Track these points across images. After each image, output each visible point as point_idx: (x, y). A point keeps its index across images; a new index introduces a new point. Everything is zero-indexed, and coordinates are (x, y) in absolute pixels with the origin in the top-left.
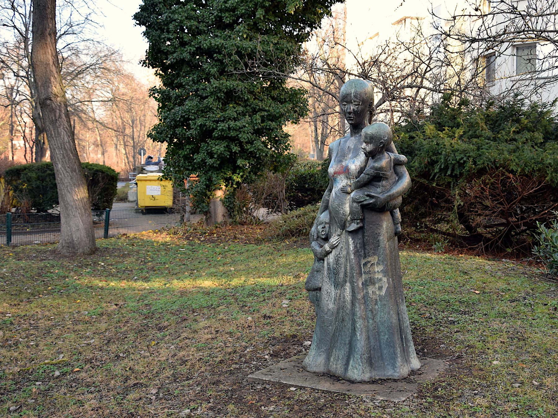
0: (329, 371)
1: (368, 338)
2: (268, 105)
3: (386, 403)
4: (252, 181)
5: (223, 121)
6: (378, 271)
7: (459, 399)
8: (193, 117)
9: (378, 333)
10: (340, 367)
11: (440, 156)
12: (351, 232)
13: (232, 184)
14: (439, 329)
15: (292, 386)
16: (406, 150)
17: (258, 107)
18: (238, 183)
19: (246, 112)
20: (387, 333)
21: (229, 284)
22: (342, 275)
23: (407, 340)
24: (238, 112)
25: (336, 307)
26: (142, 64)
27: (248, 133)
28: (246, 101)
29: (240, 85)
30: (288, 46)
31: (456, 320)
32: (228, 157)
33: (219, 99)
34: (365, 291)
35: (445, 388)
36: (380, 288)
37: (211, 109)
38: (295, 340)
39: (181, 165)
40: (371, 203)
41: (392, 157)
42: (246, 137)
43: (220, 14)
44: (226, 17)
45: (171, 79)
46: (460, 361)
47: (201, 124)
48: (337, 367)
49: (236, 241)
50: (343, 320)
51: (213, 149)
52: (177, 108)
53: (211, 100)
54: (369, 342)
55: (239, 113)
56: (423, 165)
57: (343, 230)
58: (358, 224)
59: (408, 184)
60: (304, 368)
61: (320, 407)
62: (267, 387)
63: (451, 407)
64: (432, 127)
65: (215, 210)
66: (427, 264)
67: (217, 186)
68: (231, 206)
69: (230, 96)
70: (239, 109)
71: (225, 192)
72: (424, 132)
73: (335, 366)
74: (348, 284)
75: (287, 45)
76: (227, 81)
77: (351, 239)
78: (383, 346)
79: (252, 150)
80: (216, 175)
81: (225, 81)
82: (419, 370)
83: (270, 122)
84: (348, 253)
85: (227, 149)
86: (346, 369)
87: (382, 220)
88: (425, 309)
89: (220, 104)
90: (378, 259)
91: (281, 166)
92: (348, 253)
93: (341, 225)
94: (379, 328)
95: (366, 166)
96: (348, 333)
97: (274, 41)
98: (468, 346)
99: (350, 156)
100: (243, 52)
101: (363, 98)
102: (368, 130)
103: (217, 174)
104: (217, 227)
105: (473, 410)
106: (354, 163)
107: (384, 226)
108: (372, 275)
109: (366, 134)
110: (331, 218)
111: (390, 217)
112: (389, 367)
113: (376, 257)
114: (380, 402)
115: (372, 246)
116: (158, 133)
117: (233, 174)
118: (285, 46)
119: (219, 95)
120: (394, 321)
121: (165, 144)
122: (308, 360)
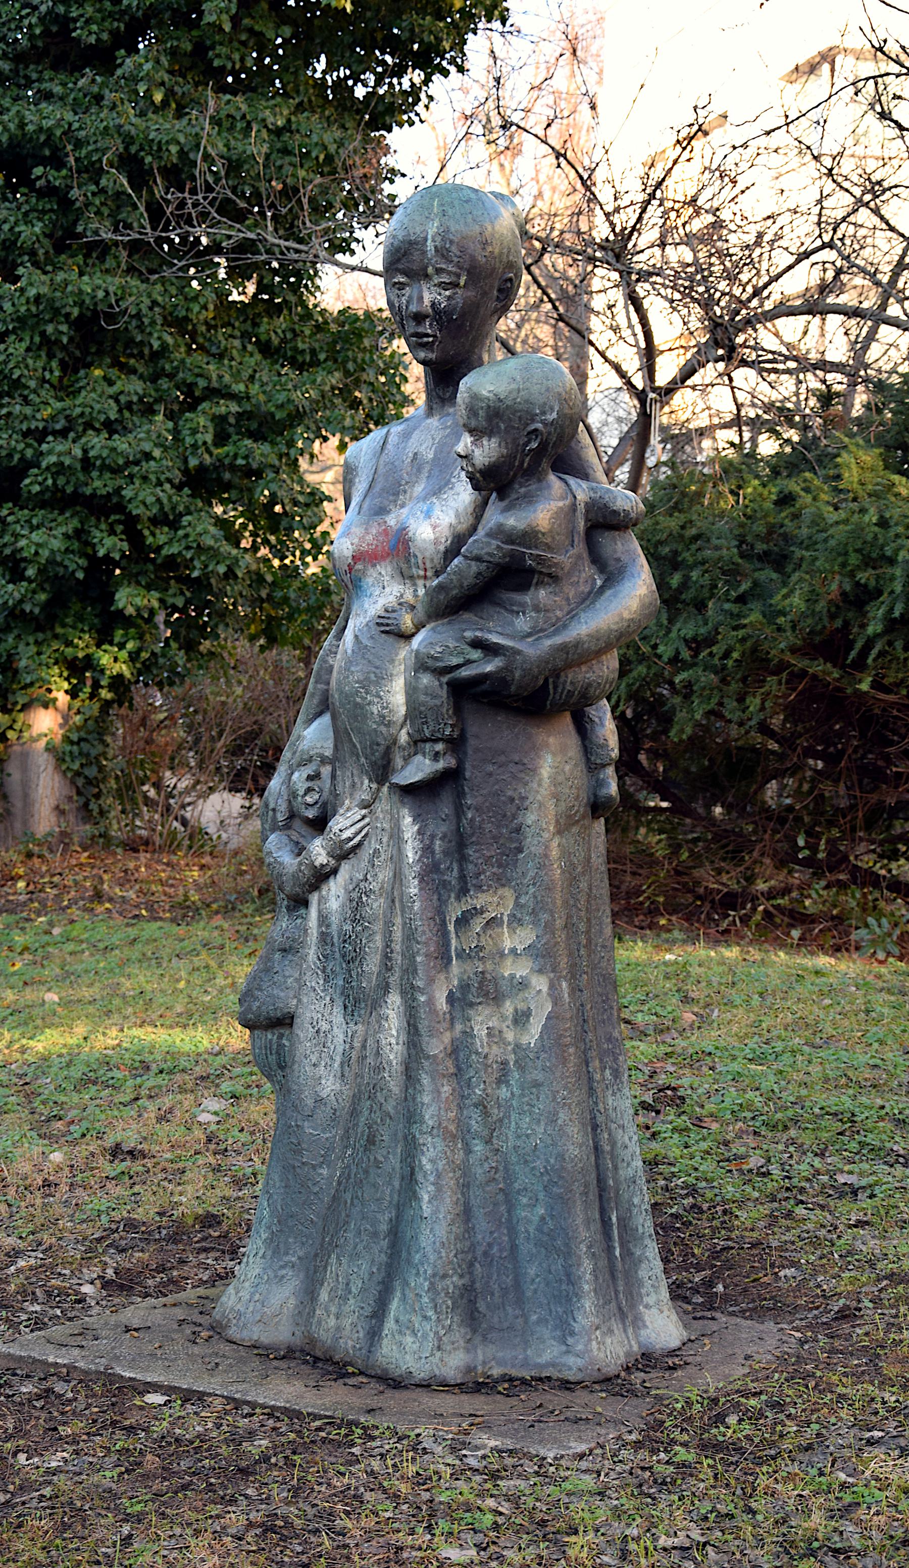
0: (312, 1341)
1: (466, 1214)
2: (245, 375)
3: (509, 1461)
4: (174, 678)
5: (63, 434)
6: (513, 951)
7: (800, 1457)
9: (508, 1197)
11: (889, 570)
12: (409, 791)
13: (96, 686)
14: (789, 1215)
15: (155, 1387)
16: (760, 547)
17: (202, 383)
18: (118, 682)
19: (158, 401)
20: (541, 1196)
21: (23, 1050)
22: (372, 964)
24: (123, 399)
25: (347, 1093)
27: (160, 484)
28: (156, 356)
29: (137, 294)
30: (327, 138)
31: (864, 1182)
32: (80, 575)
33: (48, 345)
34: (459, 1027)
35: (756, 1416)
36: (521, 1019)
37: (17, 384)
38: (217, 1237)
40: (485, 677)
41: (581, 496)
42: (150, 500)
43: (61, 9)
44: (88, 22)
46: (846, 1327)
48: (339, 1325)
49: (100, 909)
50: (371, 1141)
51: (22, 543)
54: (469, 1231)
55: (129, 406)
56: (821, 606)
57: (381, 783)
58: (436, 756)
59: (643, 606)
60: (218, 1330)
61: (244, 1464)
62: (60, 1387)
63: (763, 1481)
64: (870, 457)
65: (26, 786)
66: (802, 990)
67: (36, 692)
68: (91, 772)
69: (94, 337)
70: (130, 388)
71: (66, 718)
72: (838, 477)
73: (332, 1322)
74: (394, 999)
75: (319, 132)
76: (81, 274)
77: (408, 820)
78: (525, 1248)
79: (175, 549)
80: (33, 649)
81: (74, 276)
82: (672, 1353)
83: (248, 442)
84: (398, 877)
85: (76, 545)
86: (374, 1335)
87: (535, 749)
88: (751, 1141)
89: (54, 364)
90: (517, 904)
91: (290, 617)
92: (398, 877)
93: (373, 764)
94: (509, 1177)
95: (473, 529)
96: (389, 1192)
97: (270, 120)
98: (890, 1276)
99: (419, 489)
100: (148, 159)
101: (473, 258)
102: (482, 383)
103: (37, 643)
104: (29, 855)
105: (848, 1499)
106: (428, 515)
107: (545, 772)
108: (489, 966)
109: (475, 397)
110: (340, 736)
111: (573, 741)
112: (545, 1332)
113: (508, 893)
114: (484, 1457)
117: (98, 646)
118: (315, 138)
119: (50, 329)
120: (574, 1151)
122: (232, 1299)
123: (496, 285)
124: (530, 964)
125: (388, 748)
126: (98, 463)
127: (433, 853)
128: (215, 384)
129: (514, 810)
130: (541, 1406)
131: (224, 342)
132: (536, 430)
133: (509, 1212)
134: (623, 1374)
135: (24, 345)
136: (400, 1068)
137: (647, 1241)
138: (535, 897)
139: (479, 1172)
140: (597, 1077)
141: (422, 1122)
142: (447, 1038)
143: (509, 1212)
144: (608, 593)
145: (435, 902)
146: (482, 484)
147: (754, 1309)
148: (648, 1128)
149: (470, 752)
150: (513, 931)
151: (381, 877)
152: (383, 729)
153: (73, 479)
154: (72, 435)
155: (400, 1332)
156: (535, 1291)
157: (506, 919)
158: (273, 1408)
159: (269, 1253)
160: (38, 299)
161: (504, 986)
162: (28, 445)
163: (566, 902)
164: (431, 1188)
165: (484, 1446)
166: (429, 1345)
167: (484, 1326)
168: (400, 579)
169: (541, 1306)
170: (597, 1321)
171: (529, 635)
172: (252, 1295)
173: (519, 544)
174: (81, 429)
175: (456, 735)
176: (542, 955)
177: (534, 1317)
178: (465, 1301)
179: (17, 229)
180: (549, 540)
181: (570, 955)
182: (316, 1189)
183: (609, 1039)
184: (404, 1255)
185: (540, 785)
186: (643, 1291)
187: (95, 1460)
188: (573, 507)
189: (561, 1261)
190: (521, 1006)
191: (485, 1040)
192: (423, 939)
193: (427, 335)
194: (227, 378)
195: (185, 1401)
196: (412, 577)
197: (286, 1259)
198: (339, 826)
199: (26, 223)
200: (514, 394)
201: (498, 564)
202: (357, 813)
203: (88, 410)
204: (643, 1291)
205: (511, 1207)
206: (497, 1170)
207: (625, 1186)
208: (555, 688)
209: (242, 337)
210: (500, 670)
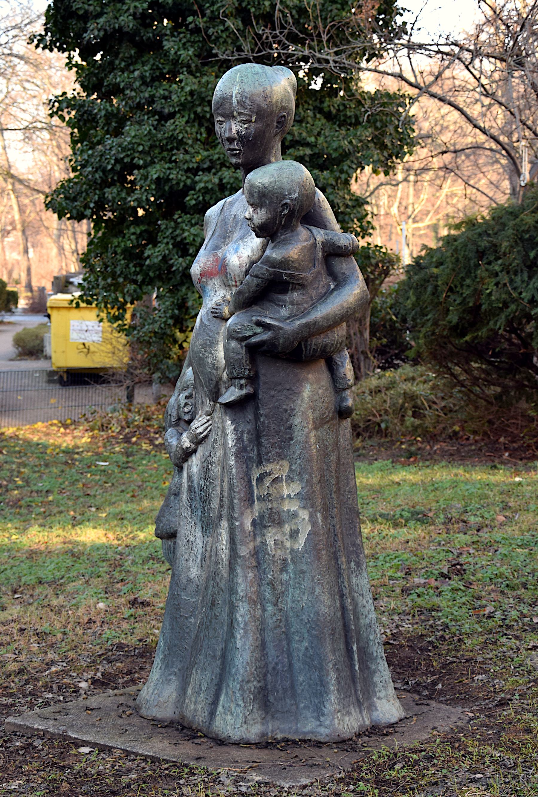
0: (183, 717)
1: (263, 646)
2: (316, 132)
5: (208, 170)
6: (289, 496)
8: (141, 162)
10: (203, 708)
12: (228, 406)
15: (86, 743)
17: (289, 138)
20: (306, 635)
22: (215, 504)
23: (365, 656)
26: (36, 42)
34: (259, 540)
36: (294, 534)
37: (181, 142)
39: (118, 270)
45: (96, 75)
47: (158, 178)
48: (196, 709)
50: (213, 604)
52: (109, 141)
53: (181, 121)
58: (241, 387)
62: (37, 743)
73: (192, 706)
74: (224, 524)
77: (229, 422)
78: (297, 665)
82: (392, 725)
86: (212, 714)
87: (300, 382)
89: (203, 130)
90: (291, 470)
93: (210, 391)
94: (288, 624)
101: (259, 106)
106: (236, 251)
108: (275, 505)
109: (252, 186)
112: (308, 714)
115: (276, 439)
116: (66, 198)
119: (199, 110)
120: (324, 610)
121: (85, 225)
123: (275, 119)
124: (298, 504)
125: (217, 382)
126: (229, 186)
127: (243, 441)
128: (297, 138)
129: (287, 416)
130: (296, 756)
131: (303, 113)
132: (286, 204)
133: (288, 645)
134: (354, 738)
135: (184, 120)
136: (227, 563)
137: (379, 661)
138: (301, 466)
139: (270, 622)
140: (344, 567)
141: (237, 593)
142: (251, 546)
143: (288, 644)
144: (335, 293)
145: (245, 469)
146: (260, 234)
147: (452, 699)
148: (437, 588)
149: (261, 384)
150: (288, 485)
151: (218, 454)
152: (214, 372)
153: (214, 196)
154: (214, 171)
155: (225, 713)
156: (303, 690)
157: (284, 478)
158: (147, 756)
159: (163, 666)
160: (192, 93)
161: (284, 516)
162: (188, 177)
163: (321, 469)
164: (242, 631)
165: (253, 780)
166: (240, 720)
167: (273, 710)
168: (223, 286)
169: (306, 699)
170: (338, 708)
171: (288, 318)
172: (154, 690)
173: (279, 268)
174: (218, 167)
175: (252, 374)
176: (306, 498)
177: (302, 705)
178: (261, 696)
179: (179, 53)
180: (296, 265)
181: (323, 498)
182: (188, 630)
183: (354, 545)
184: (227, 669)
185: (302, 401)
186: (377, 689)
187: (35, 785)
188: (314, 245)
189: (317, 673)
190: (294, 527)
191: (273, 547)
192: (237, 490)
193: (236, 150)
194: (304, 134)
195: (100, 751)
196: (229, 286)
197: (172, 670)
198: (195, 426)
199: (184, 49)
200: (273, 185)
201: (267, 279)
202: (205, 419)
203: (222, 156)
204: (377, 689)
205: (289, 641)
206: (281, 621)
207: (364, 629)
208: (306, 347)
209: (314, 109)
210: (271, 339)
